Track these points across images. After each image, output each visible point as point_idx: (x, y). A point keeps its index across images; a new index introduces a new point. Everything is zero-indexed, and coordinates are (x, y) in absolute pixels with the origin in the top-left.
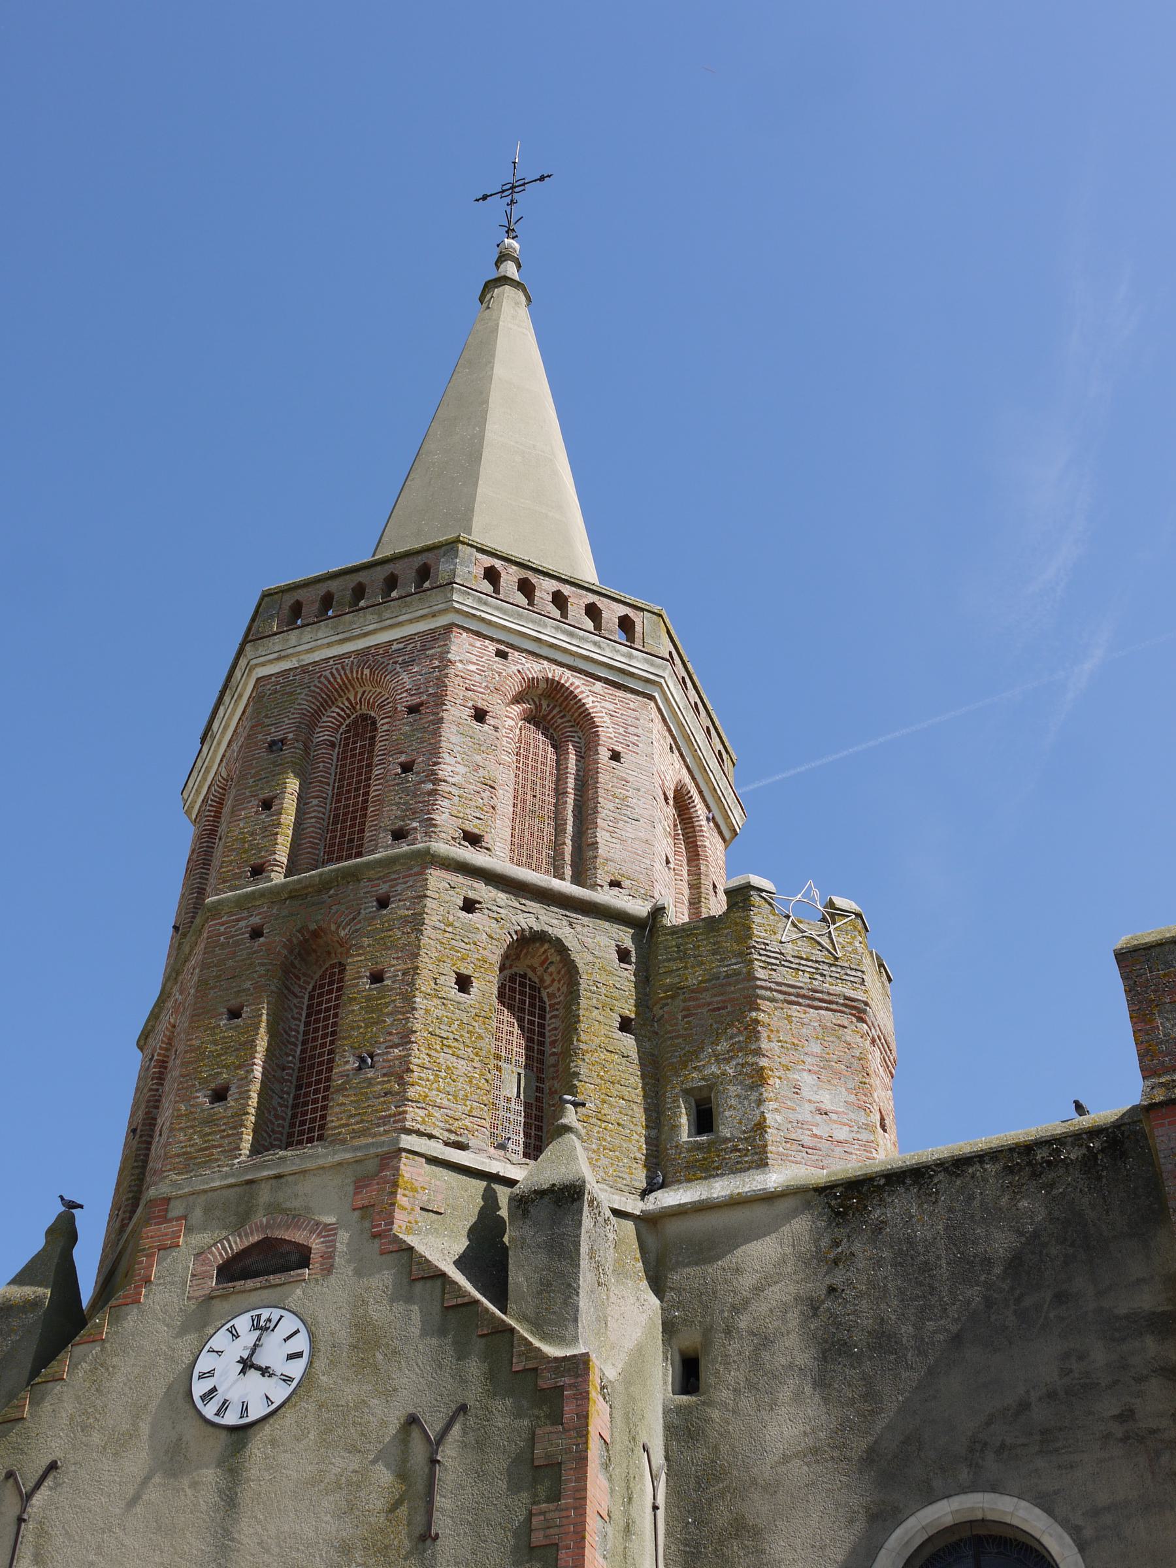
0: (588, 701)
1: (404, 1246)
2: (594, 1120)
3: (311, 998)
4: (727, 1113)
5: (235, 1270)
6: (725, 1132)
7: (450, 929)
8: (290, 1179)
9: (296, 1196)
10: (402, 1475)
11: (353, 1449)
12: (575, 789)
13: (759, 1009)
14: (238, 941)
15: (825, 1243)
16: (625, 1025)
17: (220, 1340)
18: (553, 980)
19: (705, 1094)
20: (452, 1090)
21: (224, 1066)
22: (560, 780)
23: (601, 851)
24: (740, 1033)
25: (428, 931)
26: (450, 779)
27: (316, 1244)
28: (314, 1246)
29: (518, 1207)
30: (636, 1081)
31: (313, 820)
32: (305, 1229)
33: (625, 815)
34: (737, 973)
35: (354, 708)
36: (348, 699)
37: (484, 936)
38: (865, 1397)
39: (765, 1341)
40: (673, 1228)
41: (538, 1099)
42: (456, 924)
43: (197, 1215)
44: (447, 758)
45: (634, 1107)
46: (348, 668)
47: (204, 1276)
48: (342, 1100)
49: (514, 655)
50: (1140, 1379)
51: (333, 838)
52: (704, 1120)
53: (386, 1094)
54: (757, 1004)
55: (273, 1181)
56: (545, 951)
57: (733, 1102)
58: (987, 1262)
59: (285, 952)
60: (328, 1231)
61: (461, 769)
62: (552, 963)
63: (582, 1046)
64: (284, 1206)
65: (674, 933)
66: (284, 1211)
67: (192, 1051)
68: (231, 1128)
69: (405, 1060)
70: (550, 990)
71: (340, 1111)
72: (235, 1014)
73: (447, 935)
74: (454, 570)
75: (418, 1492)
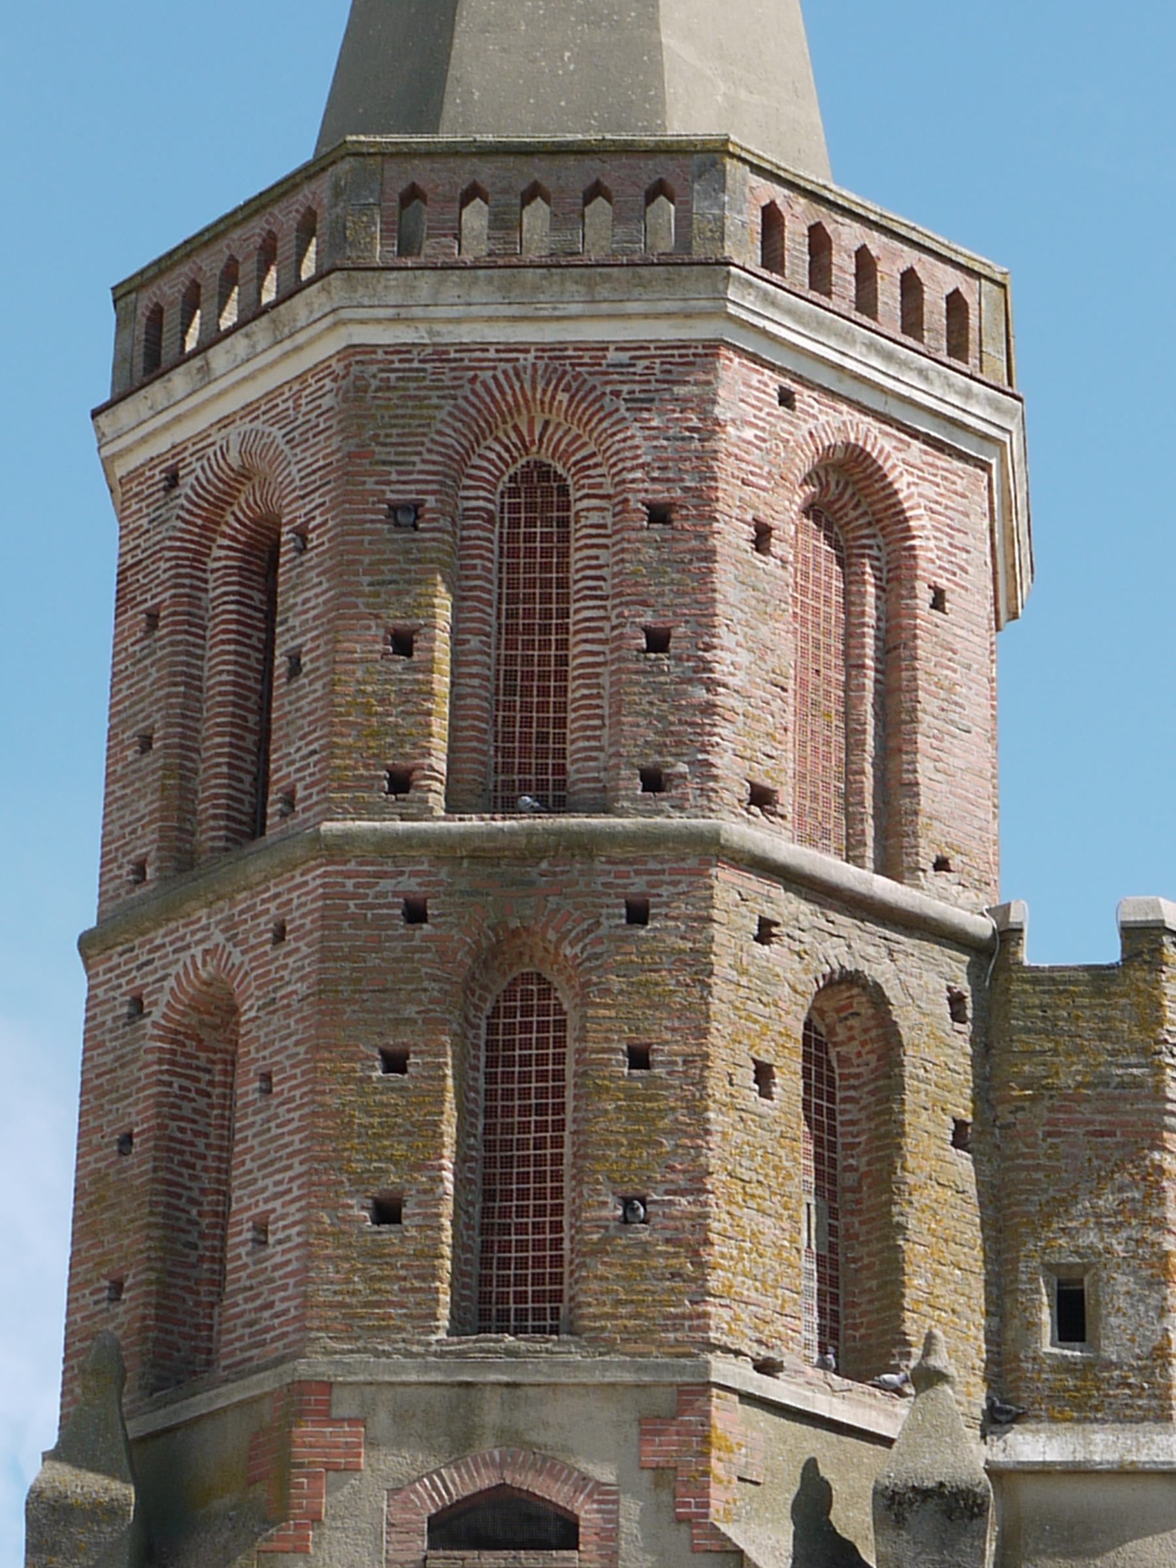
0: (903, 483)
1: (729, 1548)
2: (925, 1308)
3: (492, 1029)
4: (1113, 1320)
6: (1111, 1353)
7: (744, 981)
8: (531, 1392)
9: (546, 1425)
12: (877, 660)
13: (1164, 1149)
14: (382, 917)
16: (960, 1139)
18: (852, 1038)
19: (1074, 1275)
20: (758, 1272)
21: (390, 1159)
22: (851, 635)
23: (925, 803)
24: (1135, 1184)
25: (719, 988)
26: (730, 680)
27: (587, 1513)
28: (582, 1515)
29: (889, 1508)
30: (974, 1235)
31: (476, 682)
32: (565, 1482)
33: (952, 722)
34: (1137, 1083)
35: (526, 448)
36: (516, 428)
37: (787, 989)
40: (1031, 1493)
41: (832, 1248)
42: (752, 970)
43: (382, 1420)
44: (725, 637)
45: (971, 1278)
46: (527, 377)
47: (407, 1529)
48: (601, 1270)
49: (804, 397)
51: (509, 722)
52: (1073, 1321)
53: (673, 1275)
54: (1163, 1140)
55: (505, 1390)
56: (852, 997)
57: (1122, 1302)
59: (469, 961)
60: (601, 1492)
61: (743, 658)
62: (858, 1014)
63: (910, 1179)
64: (527, 1438)
65: (1035, 981)
66: (530, 1446)
67: (326, 1116)
68: (416, 1277)
69: (700, 1221)
70: (843, 1050)
71: (595, 1288)
72: (395, 1062)
73: (743, 992)
74: (721, 219)
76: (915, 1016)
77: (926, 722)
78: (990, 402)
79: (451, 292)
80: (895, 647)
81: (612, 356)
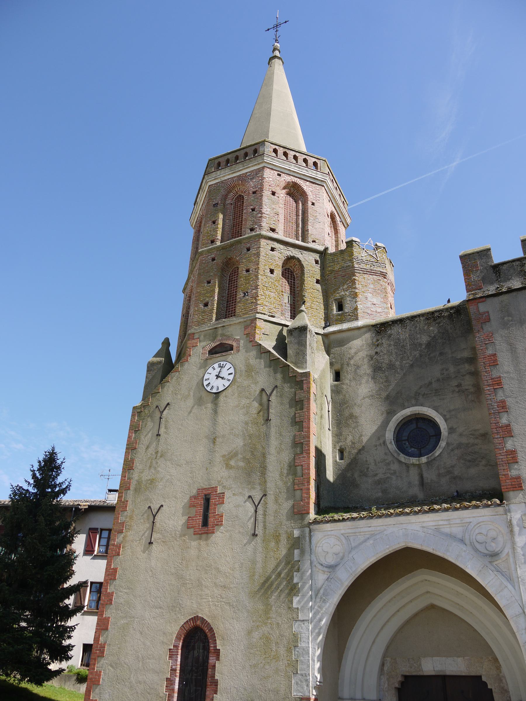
0: (305, 188)
3: (230, 277)
5: (213, 352)
9: (229, 331)
10: (261, 404)
11: (247, 398)
15: (374, 340)
16: (318, 282)
17: (210, 370)
22: (297, 211)
25: (261, 257)
27: (235, 344)
30: (321, 297)
34: (349, 266)
38: (386, 381)
39: (358, 367)
40: (332, 337)
48: (240, 305)
49: (283, 175)
50: (463, 376)
52: (340, 307)
57: (348, 302)
58: (421, 345)
60: (238, 341)
66: (225, 336)
69: (257, 293)
71: (239, 308)
75: (265, 409)
76: (307, 263)
77: (310, 221)
78: (321, 175)
79: (222, 172)
80: (305, 212)
81: (248, 174)
